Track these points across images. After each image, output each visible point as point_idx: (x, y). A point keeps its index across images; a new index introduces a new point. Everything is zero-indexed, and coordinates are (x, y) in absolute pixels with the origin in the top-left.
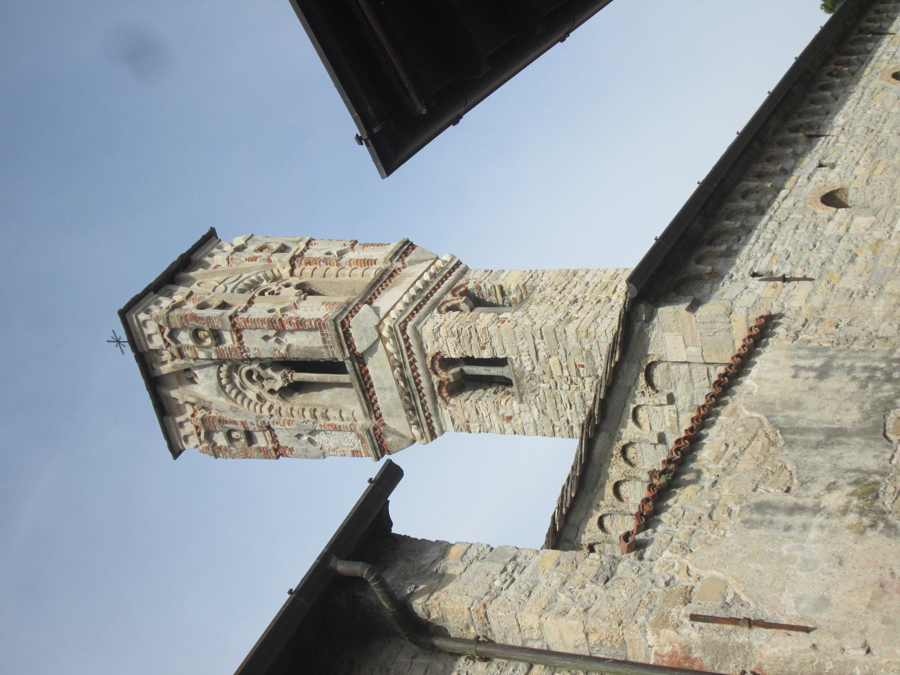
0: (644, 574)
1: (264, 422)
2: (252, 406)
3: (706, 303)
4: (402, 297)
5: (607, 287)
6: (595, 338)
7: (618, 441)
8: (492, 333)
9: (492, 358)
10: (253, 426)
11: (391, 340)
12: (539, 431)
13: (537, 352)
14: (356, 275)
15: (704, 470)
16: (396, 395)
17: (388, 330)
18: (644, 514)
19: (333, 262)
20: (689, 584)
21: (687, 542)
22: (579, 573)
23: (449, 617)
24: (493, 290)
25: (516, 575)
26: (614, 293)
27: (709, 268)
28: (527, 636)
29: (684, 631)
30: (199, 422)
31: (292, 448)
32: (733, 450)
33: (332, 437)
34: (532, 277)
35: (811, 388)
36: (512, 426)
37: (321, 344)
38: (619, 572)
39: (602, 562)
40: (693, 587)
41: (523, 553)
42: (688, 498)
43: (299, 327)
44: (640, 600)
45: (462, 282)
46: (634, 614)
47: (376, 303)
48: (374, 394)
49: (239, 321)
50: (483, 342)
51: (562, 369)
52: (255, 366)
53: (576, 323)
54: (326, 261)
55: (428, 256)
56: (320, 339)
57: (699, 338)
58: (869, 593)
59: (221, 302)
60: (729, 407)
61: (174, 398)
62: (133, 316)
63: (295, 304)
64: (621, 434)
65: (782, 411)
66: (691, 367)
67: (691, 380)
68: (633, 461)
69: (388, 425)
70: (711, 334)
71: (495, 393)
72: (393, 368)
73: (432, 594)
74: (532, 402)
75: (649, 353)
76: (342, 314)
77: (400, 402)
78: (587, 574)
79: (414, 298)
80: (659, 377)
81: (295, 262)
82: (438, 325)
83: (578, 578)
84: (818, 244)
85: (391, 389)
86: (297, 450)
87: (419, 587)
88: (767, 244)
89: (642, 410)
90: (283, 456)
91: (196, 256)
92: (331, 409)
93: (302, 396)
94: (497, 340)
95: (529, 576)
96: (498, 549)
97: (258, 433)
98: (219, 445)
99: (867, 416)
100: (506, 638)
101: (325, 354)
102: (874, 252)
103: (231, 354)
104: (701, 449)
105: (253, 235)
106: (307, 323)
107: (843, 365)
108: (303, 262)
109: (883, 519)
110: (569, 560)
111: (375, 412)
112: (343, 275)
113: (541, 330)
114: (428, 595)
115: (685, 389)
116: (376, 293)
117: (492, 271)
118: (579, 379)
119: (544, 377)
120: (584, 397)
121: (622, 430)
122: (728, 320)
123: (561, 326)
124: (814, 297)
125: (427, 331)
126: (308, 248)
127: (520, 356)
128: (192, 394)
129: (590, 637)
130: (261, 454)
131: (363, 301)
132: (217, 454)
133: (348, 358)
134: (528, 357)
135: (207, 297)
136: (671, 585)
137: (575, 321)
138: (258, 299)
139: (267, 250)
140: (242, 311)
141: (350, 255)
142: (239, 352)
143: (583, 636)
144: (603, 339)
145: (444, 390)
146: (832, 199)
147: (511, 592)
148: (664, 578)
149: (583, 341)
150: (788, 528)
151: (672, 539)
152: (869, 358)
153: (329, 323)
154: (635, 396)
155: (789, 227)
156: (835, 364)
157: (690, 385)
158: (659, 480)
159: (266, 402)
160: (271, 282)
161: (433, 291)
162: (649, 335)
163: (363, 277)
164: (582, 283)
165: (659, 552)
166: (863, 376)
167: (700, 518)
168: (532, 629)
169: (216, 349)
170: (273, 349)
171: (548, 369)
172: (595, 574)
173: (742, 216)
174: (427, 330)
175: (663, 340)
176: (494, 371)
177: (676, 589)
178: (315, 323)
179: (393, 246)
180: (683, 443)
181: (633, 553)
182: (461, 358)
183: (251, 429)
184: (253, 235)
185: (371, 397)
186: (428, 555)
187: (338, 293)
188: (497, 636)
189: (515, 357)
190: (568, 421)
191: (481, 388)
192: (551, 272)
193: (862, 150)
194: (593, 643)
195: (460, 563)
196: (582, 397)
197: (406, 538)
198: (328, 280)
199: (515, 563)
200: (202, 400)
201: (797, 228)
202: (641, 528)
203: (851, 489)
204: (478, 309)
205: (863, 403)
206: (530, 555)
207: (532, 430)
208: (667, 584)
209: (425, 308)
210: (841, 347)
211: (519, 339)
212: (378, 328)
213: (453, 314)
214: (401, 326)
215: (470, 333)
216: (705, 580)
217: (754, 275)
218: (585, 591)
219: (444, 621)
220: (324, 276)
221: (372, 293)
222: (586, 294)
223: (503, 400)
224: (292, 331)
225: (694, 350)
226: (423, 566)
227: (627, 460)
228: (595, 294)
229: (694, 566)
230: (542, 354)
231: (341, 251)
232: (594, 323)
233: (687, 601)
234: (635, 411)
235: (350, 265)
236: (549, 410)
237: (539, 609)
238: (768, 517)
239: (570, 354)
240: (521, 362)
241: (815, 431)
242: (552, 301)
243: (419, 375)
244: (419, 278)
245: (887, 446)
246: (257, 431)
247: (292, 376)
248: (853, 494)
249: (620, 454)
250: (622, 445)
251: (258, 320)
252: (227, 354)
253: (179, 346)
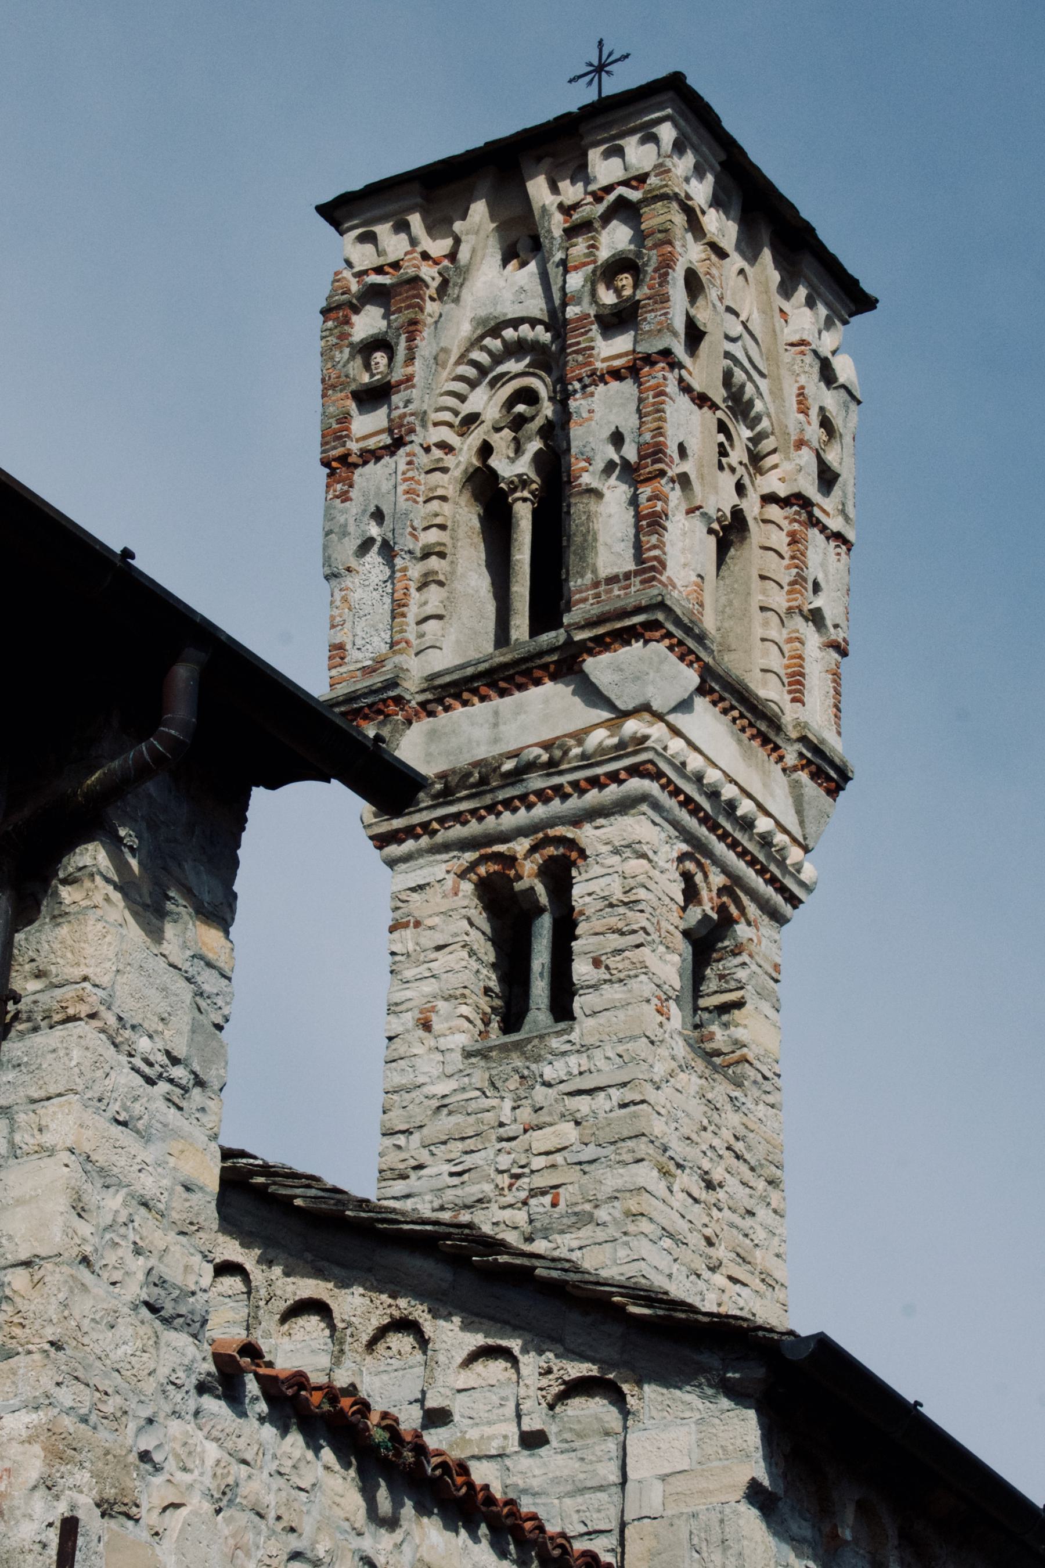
0: (167, 1397)
1: (412, 431)
3: (769, 1527)
4: (715, 766)
5: (744, 1260)
6: (625, 1233)
7: (430, 1311)
8: (633, 983)
9: (574, 985)
10: (401, 404)
11: (615, 740)
12: (395, 1097)
13: (589, 1092)
14: (766, 654)
15: (398, 1535)
16: (482, 752)
17: (639, 735)
18: (303, 1393)
19: (796, 600)
20: (143, 1512)
21: (238, 1500)
22: (169, 1238)
23: (64, 931)
24: (733, 985)
25: (163, 1087)
26: (730, 1278)
27: (848, 1535)
28: (21, 1118)
30: (411, 272)
31: (351, 500)
33: (378, 597)
34: (765, 1078)
36: (408, 1031)
37: (604, 572)
38: (171, 1336)
39: (193, 1293)
40: (137, 1521)
41: (210, 1103)
42: (338, 1499)
43: (645, 517)
44: (110, 1391)
45: (752, 909)
46: (77, 1378)
47: (701, 703)
48: (483, 699)
50: (612, 962)
51: (547, 1153)
53: (659, 1187)
55: (811, 829)
56: (616, 570)
57: (685, 1511)
59: (702, 328)
61: (468, 209)
62: (669, 111)
63: (699, 508)
64: (447, 1317)
66: (614, 1490)
67: (582, 1490)
68: (381, 1347)
69: (408, 732)
70: (695, 1541)
71: (487, 991)
72: (547, 746)
73: (117, 887)
74: (466, 1080)
75: (646, 1387)
76: (678, 622)
77: (464, 761)
78: (165, 1260)
79: (714, 795)
80: (586, 1412)
81: (796, 508)
82: (650, 854)
83: (158, 1237)
86: (343, 512)
87: (134, 856)
89: (506, 1369)
90: (329, 476)
91: (808, 265)
92: (446, 595)
93: (476, 523)
94: (618, 996)
95: (162, 1119)
96: (220, 1041)
97: (385, 416)
98: (355, 318)
100: (14, 1067)
101: (579, 581)
103: (576, 352)
104: (447, 1527)
105: (859, 402)
106: (654, 539)
108: (796, 526)
110: (198, 1214)
111: (440, 701)
112: (766, 624)
113: (643, 1102)
114: (116, 879)
115: (558, 1474)
116: (726, 704)
117: (777, 981)
118: (523, 1195)
119: (529, 1110)
120: (480, 1206)
121: (457, 1320)
123: (651, 1152)
125: (637, 827)
126: (828, 538)
127: (578, 1051)
128: (479, 253)
129: (21, 1271)
130: (333, 421)
131: (707, 673)
132: (333, 315)
133: (569, 637)
134: (576, 1072)
135: (713, 293)
136: (142, 1466)
137: (663, 1184)
138: (708, 418)
139: (826, 439)
140: (681, 380)
141: (813, 639)
142: (584, 371)
143: (23, 1256)
144: (622, 1253)
145: (493, 868)
147: (126, 1080)
148: (159, 1446)
149: (616, 1204)
151: (244, 1462)
153: (656, 592)
154: (541, 1352)
157: (569, 1488)
158: (378, 1425)
159: (462, 435)
160: (748, 449)
161: (729, 840)
162: (688, 1388)
163: (763, 670)
164: (753, 1201)
165: (215, 1433)
167: (292, 1530)
168: (40, 1130)
169: (589, 315)
170: (590, 454)
171: (548, 1119)
172: (167, 1278)
175: (679, 1421)
176: (540, 989)
177: (132, 1481)
178: (655, 558)
179: (836, 745)
180: (459, 1480)
181: (213, 1369)
182: (573, 908)
183: (395, 399)
184: (859, 402)
185: (475, 692)
186: (204, 877)
187: (723, 612)
188: (20, 1044)
189: (577, 1041)
190: (420, 1167)
191: (497, 958)
192: (776, 1125)
194: (6, 1280)
195: (189, 953)
196: (480, 1201)
197: (240, 822)
198: (753, 586)
199: (190, 1085)
200: (464, 279)
202: (271, 1386)
204: (685, 948)
206: (208, 1120)
207: (398, 1080)
208: (145, 1456)
211: (620, 1049)
212: (645, 708)
213: (676, 890)
214: (649, 766)
215: (634, 932)
216: (153, 1550)
218: (129, 1256)
219: (54, 917)
220: (763, 577)
221: (726, 695)
222: (726, 1210)
223: (470, 1009)
224: (634, 502)
226: (180, 865)
227: (381, 1333)
228: (727, 1234)
229: (184, 1522)
230: (583, 1104)
231: (823, 618)
232: (659, 1232)
233: (106, 1508)
234: (505, 1353)
235: (790, 640)
236: (446, 1123)
237: (87, 1147)
239: (585, 1173)
240: (564, 1054)
242: (711, 1128)
243: (530, 807)
244: (760, 806)
246: (389, 415)
247: (525, 500)
249: (397, 1314)
250: (421, 1321)
251: (660, 419)
252: (578, 343)
253: (597, 225)
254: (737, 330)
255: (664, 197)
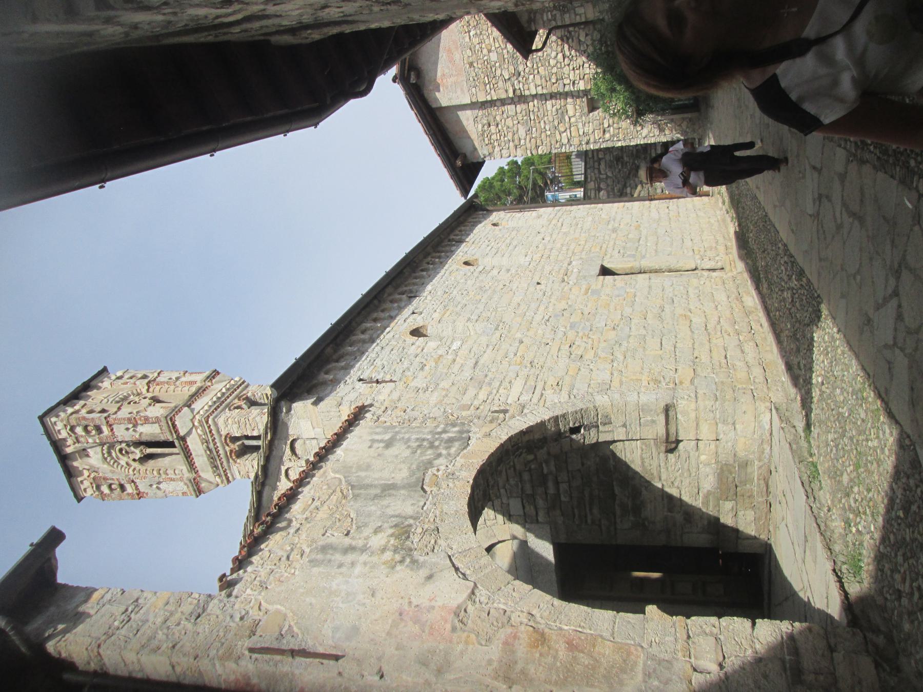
2: (123, 469)
15: (294, 519)
16: (206, 459)
25: (133, 616)
29: (243, 663)
30: (92, 480)
32: (317, 503)
35: (379, 455)
37: (160, 431)
40: (260, 620)
45: (244, 392)
47: (193, 407)
49: (111, 420)
52: (124, 445)
54: (167, 383)
55: (226, 378)
58: (390, 621)
60: (322, 471)
65: (356, 472)
72: (203, 444)
76: (171, 413)
77: (208, 463)
84: (403, 359)
85: (202, 455)
88: (372, 361)
91: (93, 383)
99: (412, 474)
102: (436, 363)
107: (403, 438)
109: (410, 555)
122: (338, 410)
124: (394, 392)
131: (185, 405)
141: (183, 379)
145: (233, 454)
146: (417, 333)
150: (340, 566)
152: (421, 432)
155: (388, 349)
156: (398, 437)
166: (415, 445)
167: (280, 559)
173: (361, 344)
174: (221, 421)
179: (207, 373)
193: (439, 303)
201: (392, 350)
203: (391, 531)
204: (253, 407)
205: (412, 464)
208: (242, 618)
209: (221, 407)
210: (405, 425)
213: (237, 411)
217: (360, 380)
224: (142, 424)
225: (319, 430)
234: (287, 471)
238: (328, 556)
241: (375, 486)
245: (422, 496)
248: (392, 535)
254: (106, 400)
255: (68, 419)
